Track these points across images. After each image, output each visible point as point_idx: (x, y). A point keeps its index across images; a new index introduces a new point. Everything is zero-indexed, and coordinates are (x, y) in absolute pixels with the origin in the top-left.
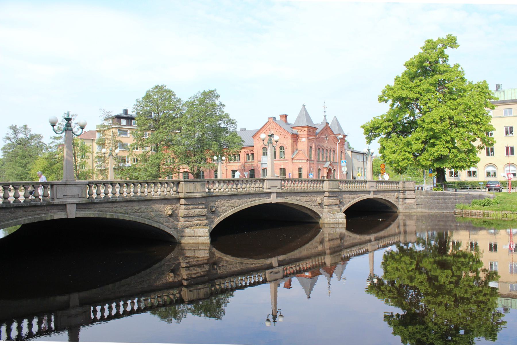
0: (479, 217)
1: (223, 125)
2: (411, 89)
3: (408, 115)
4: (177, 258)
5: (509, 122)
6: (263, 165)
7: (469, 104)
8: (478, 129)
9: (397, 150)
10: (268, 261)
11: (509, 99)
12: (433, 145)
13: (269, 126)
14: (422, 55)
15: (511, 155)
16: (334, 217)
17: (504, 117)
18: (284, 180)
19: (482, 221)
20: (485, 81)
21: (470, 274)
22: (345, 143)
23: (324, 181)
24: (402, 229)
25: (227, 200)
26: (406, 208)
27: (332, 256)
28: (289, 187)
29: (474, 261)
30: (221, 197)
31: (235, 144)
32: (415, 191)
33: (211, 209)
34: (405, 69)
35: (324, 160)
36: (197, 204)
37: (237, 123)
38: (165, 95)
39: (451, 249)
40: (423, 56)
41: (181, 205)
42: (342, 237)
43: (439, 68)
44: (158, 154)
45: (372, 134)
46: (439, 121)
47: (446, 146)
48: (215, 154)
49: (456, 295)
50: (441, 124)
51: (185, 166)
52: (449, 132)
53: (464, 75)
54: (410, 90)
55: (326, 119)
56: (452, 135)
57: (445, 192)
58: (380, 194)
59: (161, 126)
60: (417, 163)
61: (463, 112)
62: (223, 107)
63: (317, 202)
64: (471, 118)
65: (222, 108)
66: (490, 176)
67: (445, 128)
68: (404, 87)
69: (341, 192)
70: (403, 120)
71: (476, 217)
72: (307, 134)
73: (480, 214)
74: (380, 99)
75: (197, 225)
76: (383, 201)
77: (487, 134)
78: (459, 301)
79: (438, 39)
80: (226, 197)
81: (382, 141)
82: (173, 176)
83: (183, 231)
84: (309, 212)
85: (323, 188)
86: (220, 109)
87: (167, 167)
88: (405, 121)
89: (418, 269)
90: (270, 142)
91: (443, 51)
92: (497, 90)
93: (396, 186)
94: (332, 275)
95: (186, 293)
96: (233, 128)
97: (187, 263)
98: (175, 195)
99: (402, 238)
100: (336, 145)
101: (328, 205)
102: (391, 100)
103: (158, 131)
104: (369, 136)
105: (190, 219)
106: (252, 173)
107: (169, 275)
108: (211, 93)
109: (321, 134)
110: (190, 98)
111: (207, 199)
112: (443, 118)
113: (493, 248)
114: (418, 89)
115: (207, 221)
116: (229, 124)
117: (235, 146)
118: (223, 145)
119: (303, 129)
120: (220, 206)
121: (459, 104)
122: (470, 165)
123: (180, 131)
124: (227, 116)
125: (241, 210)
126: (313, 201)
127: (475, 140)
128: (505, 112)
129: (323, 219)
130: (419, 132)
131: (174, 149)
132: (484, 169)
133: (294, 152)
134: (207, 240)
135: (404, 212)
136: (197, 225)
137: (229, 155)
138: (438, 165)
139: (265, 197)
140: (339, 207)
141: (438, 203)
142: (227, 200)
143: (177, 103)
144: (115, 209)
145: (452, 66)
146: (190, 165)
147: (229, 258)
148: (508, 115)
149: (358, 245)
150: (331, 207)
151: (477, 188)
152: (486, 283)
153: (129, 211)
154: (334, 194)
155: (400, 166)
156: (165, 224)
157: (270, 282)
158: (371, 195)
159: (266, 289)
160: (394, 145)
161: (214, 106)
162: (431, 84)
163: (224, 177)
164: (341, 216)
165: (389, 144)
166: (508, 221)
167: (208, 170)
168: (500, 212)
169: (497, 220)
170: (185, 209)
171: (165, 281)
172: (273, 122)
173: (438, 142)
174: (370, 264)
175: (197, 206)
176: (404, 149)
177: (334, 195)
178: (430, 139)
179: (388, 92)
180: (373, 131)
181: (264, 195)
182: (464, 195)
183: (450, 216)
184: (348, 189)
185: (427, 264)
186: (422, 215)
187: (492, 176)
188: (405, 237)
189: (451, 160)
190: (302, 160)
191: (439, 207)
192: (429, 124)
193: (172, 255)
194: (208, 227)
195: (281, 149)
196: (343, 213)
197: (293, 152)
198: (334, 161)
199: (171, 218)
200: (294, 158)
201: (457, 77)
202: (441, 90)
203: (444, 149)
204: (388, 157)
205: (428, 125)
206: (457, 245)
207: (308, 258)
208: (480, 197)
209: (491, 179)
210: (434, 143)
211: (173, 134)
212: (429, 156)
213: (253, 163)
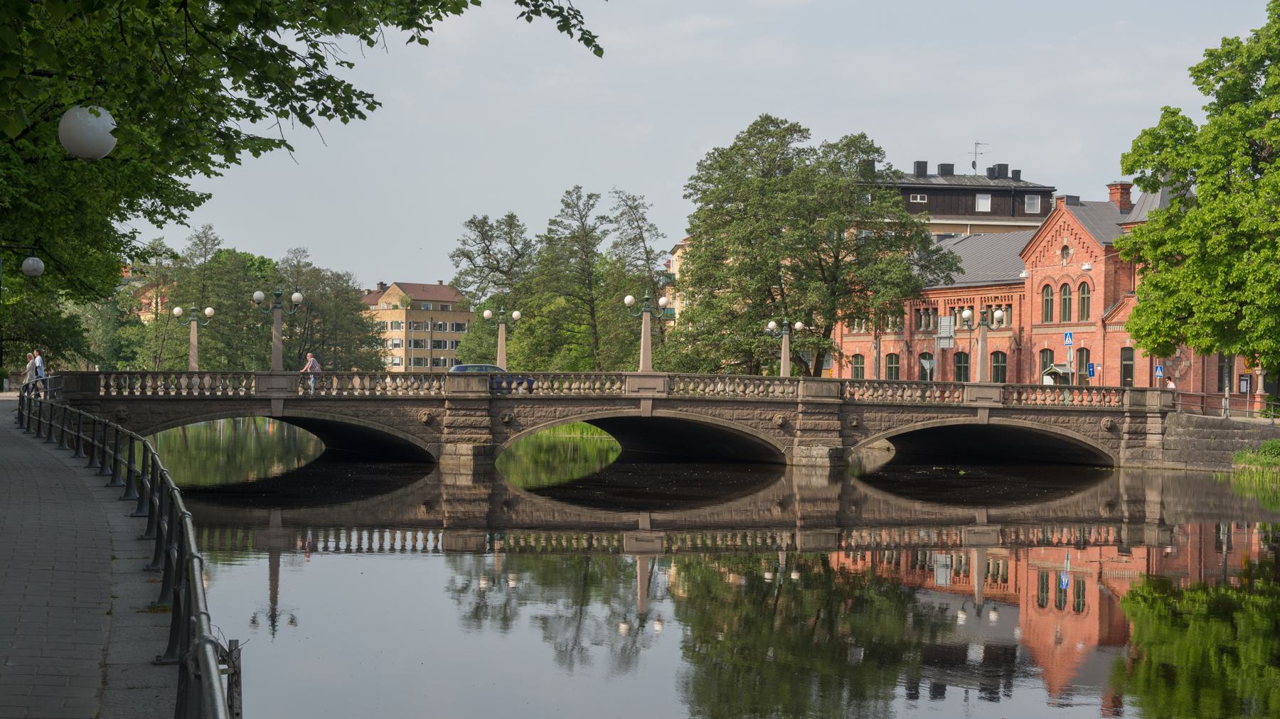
6: (942, 341)
13: (1059, 223)
30: (527, 402)
120: (523, 414)
153: (361, 413)
170: (450, 415)
171: (412, 516)
175: (472, 413)
181: (624, 403)
203: (438, 336)
207: (732, 527)
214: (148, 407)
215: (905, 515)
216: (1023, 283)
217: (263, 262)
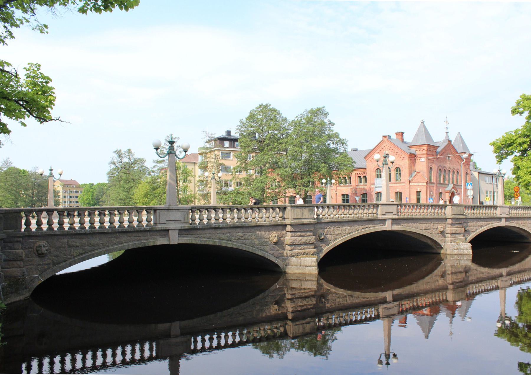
1: (332, 146)
13: (383, 146)
16: (458, 248)
22: (471, 163)
25: (337, 227)
28: (406, 212)
30: (331, 224)
31: (345, 165)
33: (319, 237)
35: (446, 182)
36: (304, 231)
37: (347, 143)
38: (270, 114)
41: (287, 232)
42: (467, 271)
45: (504, 152)
48: (324, 177)
51: (291, 190)
55: (448, 136)
58: (513, 222)
59: (266, 148)
62: (332, 126)
65: (332, 127)
69: (466, 218)
72: (427, 154)
74: (514, 112)
75: (304, 254)
80: (336, 224)
81: (516, 160)
84: (429, 242)
85: (445, 214)
86: (329, 127)
87: (271, 191)
90: (385, 163)
95: (291, 328)
98: (281, 221)
101: (451, 234)
104: (499, 154)
105: (297, 247)
106: (364, 197)
108: (319, 111)
115: (315, 250)
116: (338, 144)
117: (345, 168)
118: (332, 167)
123: (286, 152)
124: (337, 135)
125: (352, 238)
126: (434, 229)
131: (279, 172)
134: (315, 270)
139: (379, 224)
140: (464, 236)
142: (337, 227)
144: (218, 236)
146: (297, 189)
147: (340, 291)
150: (455, 235)
153: (233, 238)
154: (457, 221)
156: (270, 252)
158: (502, 223)
159: (379, 325)
161: (322, 125)
163: (334, 202)
164: (466, 246)
165: (524, 164)
170: (291, 236)
171: (264, 315)
175: (304, 234)
177: (458, 223)
179: (523, 103)
181: (378, 222)
190: (421, 182)
193: (277, 285)
194: (316, 256)
195: (397, 171)
196: (469, 243)
197: (410, 174)
198: (457, 183)
199: (276, 246)
200: (411, 180)
204: (524, 178)
213: (365, 187)
214: (66, 241)
216: (366, 168)
217: (24, 171)
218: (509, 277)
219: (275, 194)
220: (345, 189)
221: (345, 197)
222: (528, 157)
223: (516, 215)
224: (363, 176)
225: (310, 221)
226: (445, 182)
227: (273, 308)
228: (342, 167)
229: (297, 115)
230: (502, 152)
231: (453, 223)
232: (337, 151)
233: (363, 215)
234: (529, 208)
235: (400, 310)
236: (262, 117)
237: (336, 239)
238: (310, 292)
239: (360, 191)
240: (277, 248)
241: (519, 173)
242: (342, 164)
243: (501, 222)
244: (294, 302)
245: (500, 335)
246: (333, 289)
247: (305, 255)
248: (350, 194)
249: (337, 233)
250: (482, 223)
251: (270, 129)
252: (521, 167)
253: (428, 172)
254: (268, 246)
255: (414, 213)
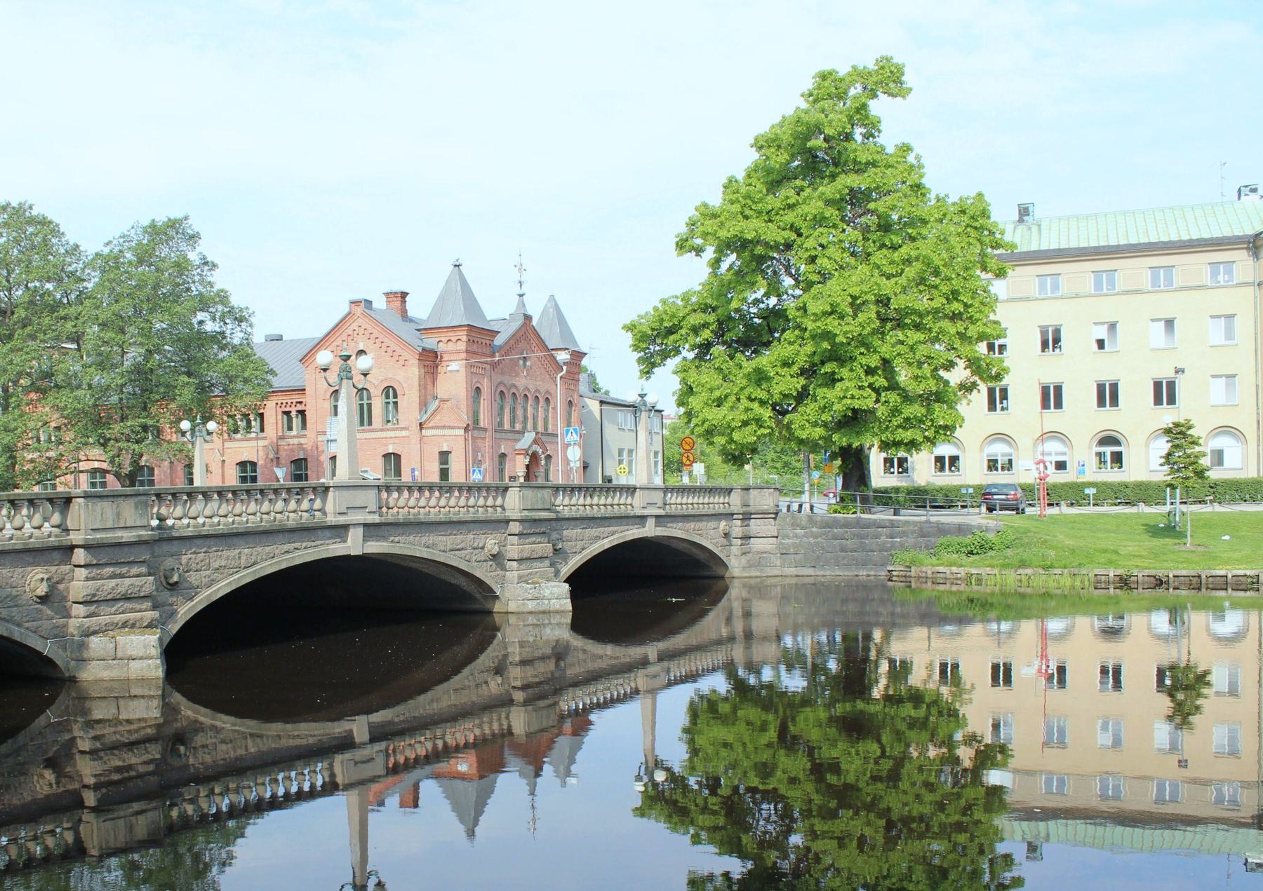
0: (954, 588)
1: (210, 327)
2: (769, 216)
3: (762, 291)
4: (64, 727)
5: (1049, 314)
7: (937, 261)
8: (958, 333)
9: (726, 396)
10: (338, 728)
11: (1051, 248)
12: (832, 380)
13: (351, 328)
14: (803, 115)
15: (1111, 406)
16: (538, 595)
17: (1037, 299)
18: (387, 486)
19: (964, 597)
20: (980, 195)
21: (932, 752)
22: (583, 377)
23: (506, 489)
24: (739, 627)
25: (214, 549)
26: (750, 565)
27: (530, 708)
28: (403, 506)
29: (940, 714)
30: (199, 542)
31: (246, 381)
32: (776, 514)
33: (166, 578)
34: (753, 156)
35: (518, 427)
36: (124, 563)
37: (253, 319)
38: (32, 234)
39: (883, 682)
40: (805, 118)
41: (76, 566)
42: (560, 653)
43: (852, 156)
44: (10, 417)
45: (657, 348)
46: (850, 311)
47: (866, 384)
48: (188, 413)
49: (889, 809)
50: (854, 320)
51: (96, 452)
52: (876, 342)
53: (921, 176)
54: (766, 218)
55: (524, 305)
56: (884, 349)
57: (863, 516)
58: (675, 526)
59: (19, 331)
60: (784, 432)
61: (917, 285)
62: (210, 270)
63: (486, 550)
64: (937, 303)
65: (209, 274)
66: (996, 469)
67: (865, 332)
68: (751, 209)
69: (558, 520)
70: (745, 308)
71: (947, 587)
72: (467, 351)
73: (957, 579)
74: (682, 245)
75: (125, 625)
76: (685, 545)
77: (991, 347)
78: (897, 828)
79: (851, 69)
80: (212, 541)
81: (685, 371)
82: (58, 484)
83: (82, 646)
84: (462, 582)
85: (504, 509)
86: (201, 275)
87: (36, 455)
88: (754, 310)
89: (787, 740)
90: (346, 374)
91: (864, 106)
92: (1021, 220)
93: (721, 500)
94: (541, 769)
95: (94, 831)
96: (242, 335)
97: (96, 738)
98: (56, 536)
99: (738, 653)
100: (555, 382)
101: (520, 560)
102: (713, 248)
103: (9, 346)
104: (646, 354)
105: (104, 609)
106: (300, 467)
107: (42, 776)
108: (172, 227)
109: (508, 348)
110: (107, 244)
111: (156, 549)
112: (858, 302)
113: (1002, 675)
114: (790, 217)
115: (155, 614)
116: (228, 321)
117: (248, 388)
118: (208, 387)
119: (453, 336)
121: (908, 262)
122: (935, 437)
123: (78, 345)
124: (223, 297)
125: (257, 577)
126: (474, 549)
127: (950, 366)
128: (1040, 283)
129: (503, 600)
130: (791, 343)
131: (58, 401)
132: (981, 450)
133: (426, 405)
134: (155, 668)
135: (746, 577)
136: (125, 625)
137: (229, 416)
138: (844, 439)
139: (329, 539)
140: (552, 565)
141: (843, 550)
142: (214, 549)
143: (68, 259)
145: (890, 150)
146: (109, 448)
147: (226, 722)
148: (1162, 287)
149: (609, 674)
150: (528, 564)
151: (959, 504)
152: (976, 773)
154: (534, 526)
155: (735, 442)
156: (27, 625)
157: (348, 787)
158: (647, 528)
159: (337, 809)
160: (719, 382)
161: (181, 266)
162: (829, 203)
163: (215, 481)
164: (556, 590)
165: (704, 378)
166: (1031, 596)
167: (167, 463)
168: (1013, 570)
169: (1003, 594)
170: (87, 579)
171: (28, 797)
172: (364, 315)
173: (845, 373)
174: (645, 732)
175: (124, 570)
176: (747, 392)
177: (537, 531)
178: (823, 363)
179: (702, 224)
180: (659, 341)
181: (327, 533)
182: (915, 523)
183: (876, 586)
184: (581, 512)
185: (810, 724)
186: (796, 584)
187: (1003, 468)
188: (748, 647)
189: (880, 422)
190: (450, 427)
191: (845, 561)
192: (819, 319)
193: (51, 716)
194: (159, 630)
195: (387, 397)
196: (565, 582)
197: (423, 405)
198: (546, 429)
199: (44, 608)
200: (425, 422)
201: (904, 182)
202: (858, 220)
203: (861, 392)
204: (701, 416)
205: (815, 321)
206: (900, 670)
208: (961, 530)
209: (1000, 478)
210: (833, 373)
211: (56, 353)
212: (820, 412)
213: (303, 441)
215: (603, 664)
216: (304, 390)
218: (665, 664)
219: (47, 465)
220: (248, 448)
221: (247, 468)
222: (713, 363)
223: (682, 509)
224: (298, 411)
225: (139, 536)
226: (514, 427)
227: (41, 781)
228: (239, 385)
229: (111, 239)
230: (651, 347)
231: (525, 532)
232: (224, 342)
233: (245, 519)
234: (711, 489)
235: (390, 765)
236: (9, 240)
237: (212, 582)
238: (144, 728)
239: (288, 452)
240: (49, 612)
241: (692, 402)
242: (237, 376)
243: (644, 527)
244: (101, 758)
245: (647, 811)
246: (204, 716)
247: (127, 630)
248: (261, 462)
249: (216, 565)
250: (599, 529)
251: (31, 277)
252: (696, 387)
253: (471, 400)
254: (20, 608)
255: (424, 507)
